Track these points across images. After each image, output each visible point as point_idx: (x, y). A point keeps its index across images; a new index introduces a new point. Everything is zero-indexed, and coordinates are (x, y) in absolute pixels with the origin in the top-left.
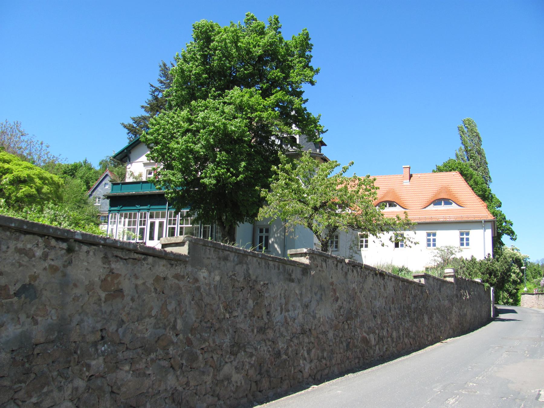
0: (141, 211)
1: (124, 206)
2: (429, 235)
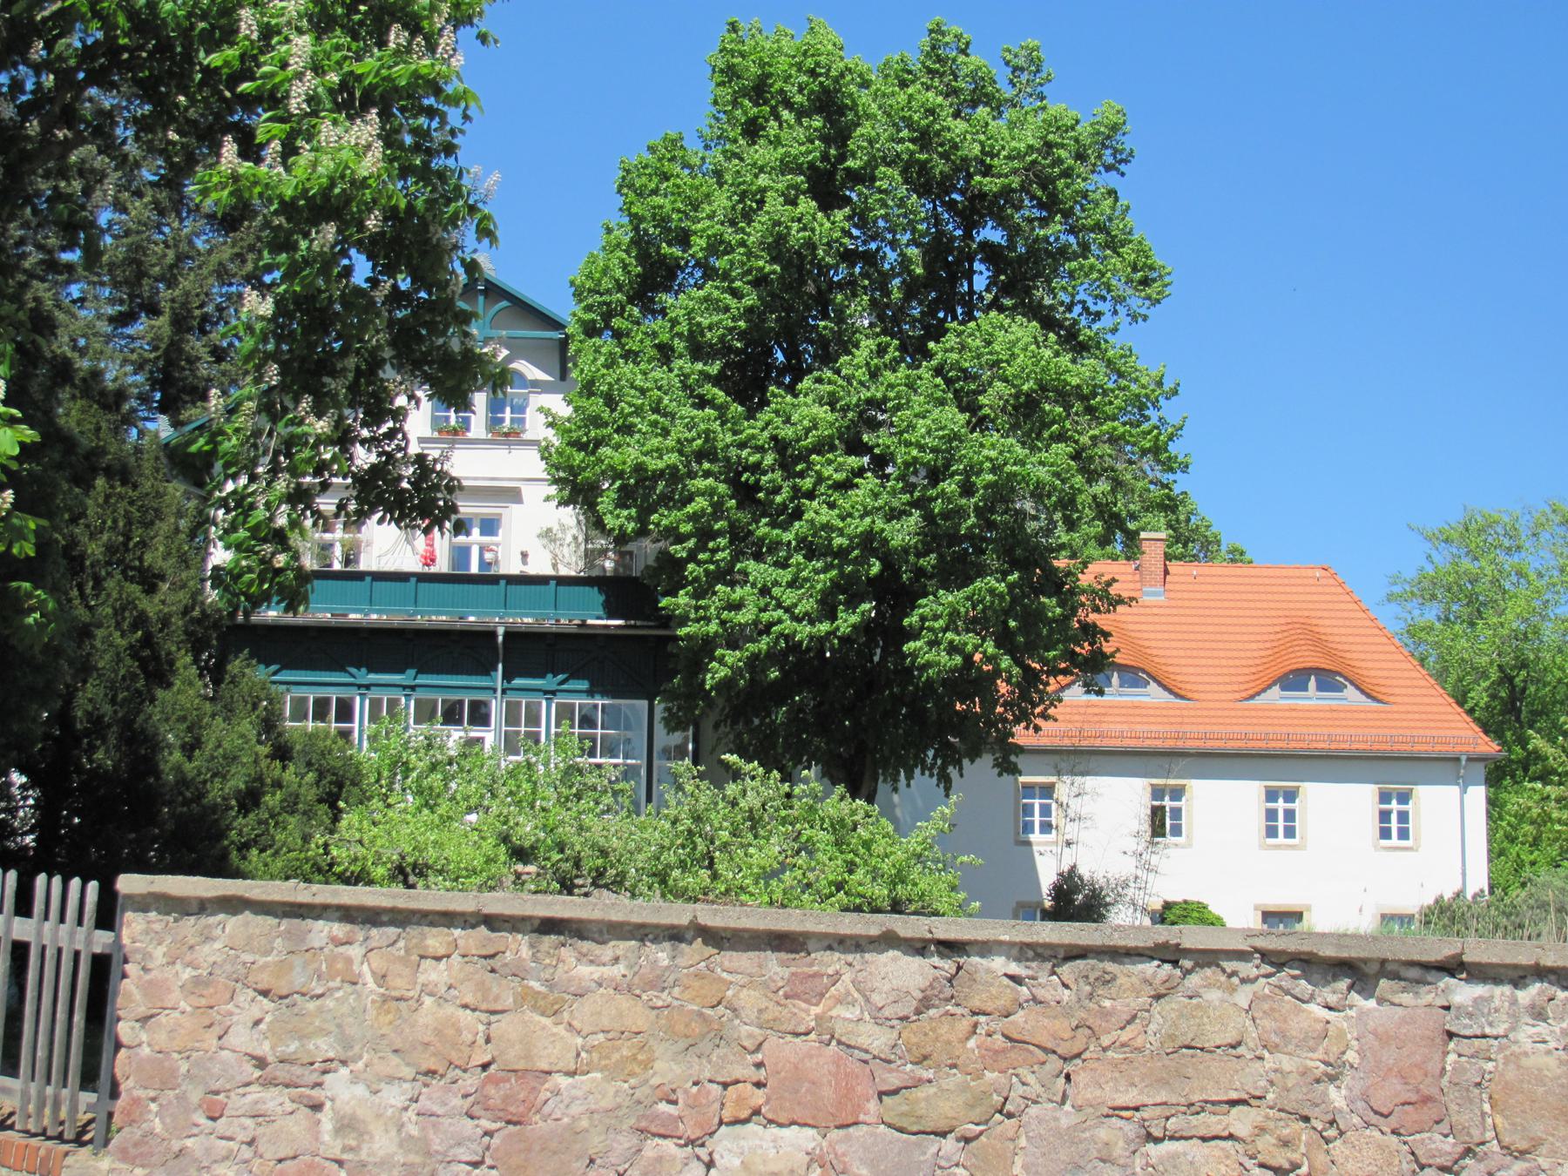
0: (374, 693)
1: (287, 666)
2: (1271, 795)
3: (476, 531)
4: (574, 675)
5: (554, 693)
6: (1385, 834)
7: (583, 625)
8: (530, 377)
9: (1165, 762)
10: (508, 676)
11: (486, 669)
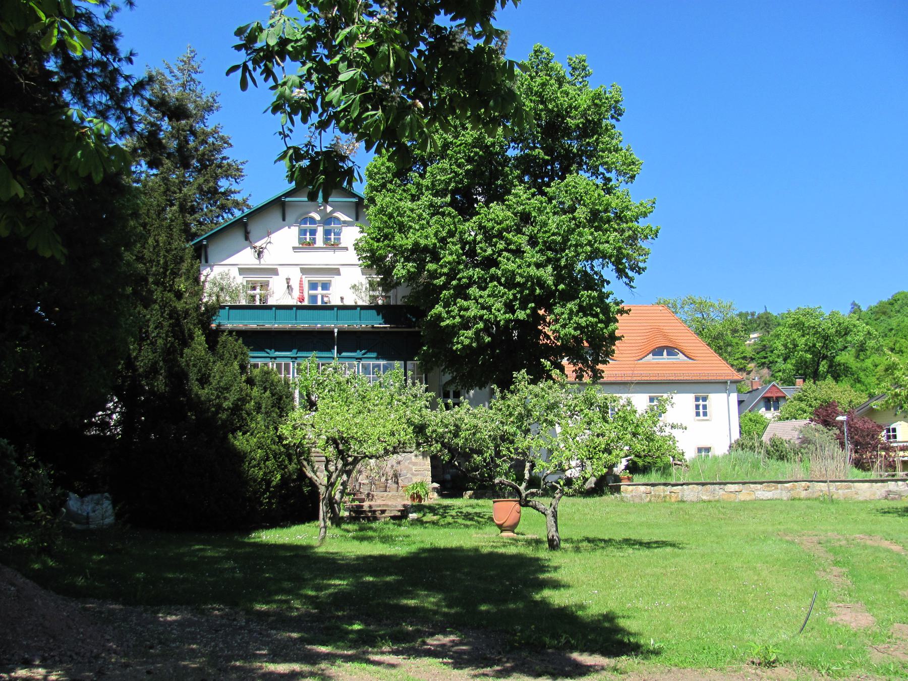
0: (278, 361)
3: (320, 288)
4: (370, 350)
5: (360, 359)
6: (698, 414)
7: (373, 327)
8: (342, 219)
9: (622, 387)
10: (339, 352)
11: (330, 349)
